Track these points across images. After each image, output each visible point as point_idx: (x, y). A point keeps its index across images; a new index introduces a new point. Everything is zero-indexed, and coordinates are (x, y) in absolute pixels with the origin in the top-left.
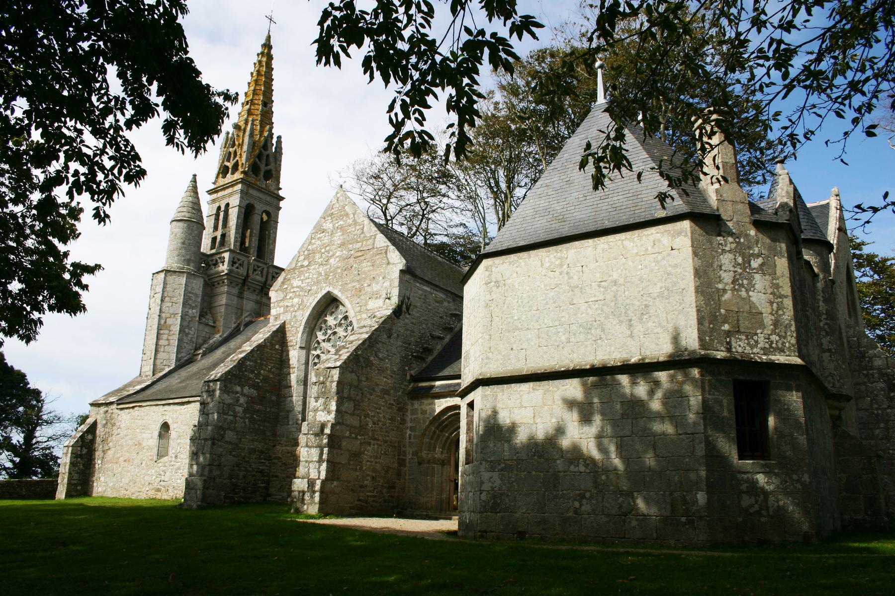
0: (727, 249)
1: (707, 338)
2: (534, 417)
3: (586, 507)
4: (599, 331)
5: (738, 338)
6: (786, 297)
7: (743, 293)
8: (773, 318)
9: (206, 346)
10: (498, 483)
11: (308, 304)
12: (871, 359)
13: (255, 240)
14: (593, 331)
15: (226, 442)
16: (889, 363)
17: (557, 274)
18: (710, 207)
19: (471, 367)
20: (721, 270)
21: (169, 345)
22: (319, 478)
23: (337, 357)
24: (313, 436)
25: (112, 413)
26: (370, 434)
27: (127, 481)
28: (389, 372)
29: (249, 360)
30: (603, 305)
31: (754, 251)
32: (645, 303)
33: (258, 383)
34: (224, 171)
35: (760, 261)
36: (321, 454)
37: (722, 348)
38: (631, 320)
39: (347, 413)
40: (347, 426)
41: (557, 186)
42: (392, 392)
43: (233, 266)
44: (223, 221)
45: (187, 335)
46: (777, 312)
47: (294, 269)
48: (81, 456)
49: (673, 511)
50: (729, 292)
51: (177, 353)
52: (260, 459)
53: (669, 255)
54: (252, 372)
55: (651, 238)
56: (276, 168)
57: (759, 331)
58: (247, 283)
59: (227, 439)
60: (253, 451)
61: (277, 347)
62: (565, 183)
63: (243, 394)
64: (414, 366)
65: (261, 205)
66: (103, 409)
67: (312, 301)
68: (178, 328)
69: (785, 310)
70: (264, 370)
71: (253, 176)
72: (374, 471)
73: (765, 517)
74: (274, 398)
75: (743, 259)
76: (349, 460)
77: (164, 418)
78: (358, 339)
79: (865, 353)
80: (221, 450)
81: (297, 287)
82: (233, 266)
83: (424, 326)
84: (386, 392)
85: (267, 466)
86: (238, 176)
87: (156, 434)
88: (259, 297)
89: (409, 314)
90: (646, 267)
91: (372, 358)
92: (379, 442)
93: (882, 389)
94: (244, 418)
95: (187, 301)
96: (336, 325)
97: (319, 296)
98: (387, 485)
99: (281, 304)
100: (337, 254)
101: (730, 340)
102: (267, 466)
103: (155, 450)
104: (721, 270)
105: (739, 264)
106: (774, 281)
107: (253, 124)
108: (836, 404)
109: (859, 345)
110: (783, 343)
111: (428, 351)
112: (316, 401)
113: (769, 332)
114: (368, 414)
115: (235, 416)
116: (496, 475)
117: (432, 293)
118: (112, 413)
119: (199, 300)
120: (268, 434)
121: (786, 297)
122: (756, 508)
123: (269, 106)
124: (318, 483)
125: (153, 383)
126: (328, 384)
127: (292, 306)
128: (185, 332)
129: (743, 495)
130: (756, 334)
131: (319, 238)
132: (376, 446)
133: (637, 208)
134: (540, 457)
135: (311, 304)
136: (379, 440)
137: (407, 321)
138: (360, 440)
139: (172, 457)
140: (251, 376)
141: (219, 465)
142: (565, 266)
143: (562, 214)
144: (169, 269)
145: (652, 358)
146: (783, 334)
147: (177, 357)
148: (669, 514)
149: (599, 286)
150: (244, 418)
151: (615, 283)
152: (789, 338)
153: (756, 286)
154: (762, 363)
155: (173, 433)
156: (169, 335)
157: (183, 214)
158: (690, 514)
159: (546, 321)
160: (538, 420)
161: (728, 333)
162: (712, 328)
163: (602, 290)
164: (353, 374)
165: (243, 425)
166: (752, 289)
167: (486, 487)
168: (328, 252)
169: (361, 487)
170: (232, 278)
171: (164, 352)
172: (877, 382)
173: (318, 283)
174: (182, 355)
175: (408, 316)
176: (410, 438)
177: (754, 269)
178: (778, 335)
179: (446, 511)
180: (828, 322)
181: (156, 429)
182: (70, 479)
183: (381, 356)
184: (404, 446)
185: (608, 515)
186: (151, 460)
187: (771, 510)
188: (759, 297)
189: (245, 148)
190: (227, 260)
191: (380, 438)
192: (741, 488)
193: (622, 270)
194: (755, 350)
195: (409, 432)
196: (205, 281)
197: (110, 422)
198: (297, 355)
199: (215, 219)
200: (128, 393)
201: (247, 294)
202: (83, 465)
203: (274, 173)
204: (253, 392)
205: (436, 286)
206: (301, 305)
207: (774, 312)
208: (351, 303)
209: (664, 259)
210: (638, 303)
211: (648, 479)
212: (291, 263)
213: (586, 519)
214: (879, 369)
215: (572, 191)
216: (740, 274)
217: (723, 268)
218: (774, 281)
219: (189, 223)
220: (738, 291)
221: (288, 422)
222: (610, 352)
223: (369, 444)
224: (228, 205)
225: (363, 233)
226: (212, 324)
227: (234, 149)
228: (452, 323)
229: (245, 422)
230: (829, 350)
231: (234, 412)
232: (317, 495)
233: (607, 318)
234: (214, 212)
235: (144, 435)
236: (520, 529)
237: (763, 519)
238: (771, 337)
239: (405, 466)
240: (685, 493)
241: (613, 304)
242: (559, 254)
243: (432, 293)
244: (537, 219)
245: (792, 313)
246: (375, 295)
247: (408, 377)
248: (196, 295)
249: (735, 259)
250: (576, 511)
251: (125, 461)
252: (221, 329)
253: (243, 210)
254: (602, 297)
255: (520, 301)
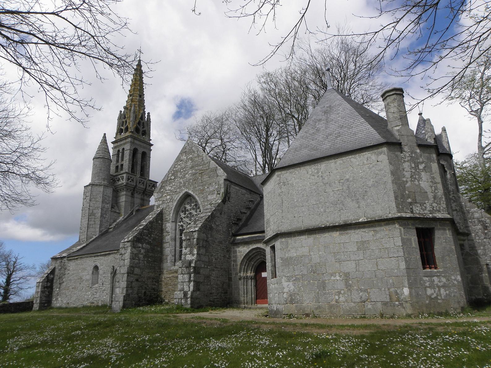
0: (406, 160)
1: (400, 206)
2: (310, 251)
3: (342, 299)
4: (341, 206)
5: (416, 206)
6: (439, 183)
7: (416, 182)
8: (433, 194)
9: (115, 223)
10: (292, 287)
11: (175, 199)
12: (473, 213)
13: (139, 167)
14: (338, 206)
15: (135, 274)
16: (483, 215)
17: (316, 177)
18: (396, 139)
19: (272, 227)
20: (404, 171)
21: (95, 224)
22: (189, 291)
23: (195, 225)
24: (185, 268)
25: (65, 263)
26: (214, 265)
27: (74, 299)
28: (221, 232)
29: (145, 229)
30: (342, 192)
31: (420, 160)
32: (365, 190)
33: (151, 241)
34: (120, 131)
35: (423, 165)
36: (190, 277)
37: (409, 211)
38: (358, 199)
39: (202, 254)
40: (203, 261)
41: (311, 132)
42: (223, 242)
43: (128, 181)
44: (121, 157)
45: (105, 218)
46: (434, 191)
47: (167, 181)
48: (47, 287)
49: (390, 299)
50: (409, 182)
51: (100, 228)
52: (153, 282)
53: (376, 165)
54: (147, 236)
55: (366, 156)
56: (148, 130)
57: (426, 202)
58: (136, 189)
59: (135, 272)
60: (149, 278)
61: (159, 222)
62: (315, 131)
63: (143, 248)
64: (233, 228)
65: (141, 149)
66: (58, 262)
67: (177, 197)
68: (100, 214)
69: (438, 190)
70: (153, 235)
71: (136, 133)
72: (217, 285)
73: (440, 300)
74: (159, 249)
75: (415, 165)
76: (204, 280)
77: (95, 263)
78: (205, 216)
79: (469, 211)
80: (133, 278)
81: (168, 190)
82: (128, 181)
83: (237, 207)
84: (220, 242)
85: (156, 286)
86: (128, 134)
87: (91, 272)
88: (142, 196)
89: (229, 202)
90: (364, 171)
91: (213, 225)
92: (219, 269)
93: (480, 229)
94: (143, 261)
95: (104, 200)
96: (190, 209)
97: (181, 194)
98: (223, 292)
99: (160, 199)
100: (190, 172)
101: (412, 207)
102: (156, 286)
103: (90, 281)
104: (404, 171)
105: (413, 168)
106: (432, 175)
107: (135, 107)
108: (462, 238)
109: (466, 207)
110: (439, 207)
111: (239, 220)
112: (186, 250)
113: (432, 202)
114: (213, 255)
115: (139, 260)
116: (291, 283)
117: (240, 190)
118: (65, 263)
119: (111, 199)
120: (157, 268)
121: (439, 183)
122: (435, 295)
123: (142, 97)
124: (189, 293)
125: (87, 245)
126: (192, 240)
127: (167, 200)
128: (103, 216)
129: (427, 288)
130: (425, 203)
131: (179, 165)
132: (217, 271)
133: (356, 141)
134: (314, 273)
135: (177, 198)
136: (218, 268)
137: (228, 205)
138: (210, 268)
139: (100, 284)
140: (147, 238)
141: (131, 287)
142: (320, 173)
143: (316, 146)
144: (93, 183)
145: (371, 218)
146: (439, 203)
147: (99, 230)
148: (389, 301)
149: (339, 182)
150: (143, 261)
151: (348, 180)
152: (442, 205)
153: (423, 178)
154: (430, 218)
155: (101, 272)
156: (95, 219)
157: (100, 154)
158: (401, 300)
159: (312, 201)
160: (312, 253)
161: (411, 204)
162: (402, 201)
163: (341, 184)
164: (204, 234)
165: (144, 264)
166: (421, 180)
167: (286, 290)
168: (185, 171)
169: (211, 294)
170: (127, 187)
171: (92, 228)
172: (477, 225)
173: (180, 187)
174: (103, 229)
175: (229, 203)
176: (233, 266)
177: (421, 170)
178: (436, 203)
179: (254, 304)
180: (454, 195)
181: (90, 269)
182: (41, 301)
183: (217, 224)
184: (231, 270)
185: (355, 302)
186: (88, 287)
187: (443, 296)
188: (425, 183)
189: (131, 119)
190: (125, 178)
191: (219, 267)
192: (426, 285)
193: (351, 174)
194: (425, 212)
195: (233, 263)
196: (113, 189)
197: (64, 268)
198: (170, 225)
199: (117, 157)
200: (73, 251)
201: (136, 195)
202: (48, 292)
203: (147, 132)
204: (148, 246)
205: (242, 186)
206: (172, 200)
207: (433, 192)
208: (199, 197)
209: (373, 166)
210: (361, 190)
211: (375, 282)
212: (164, 178)
213: (343, 305)
214: (478, 219)
215: (320, 135)
216: (414, 173)
217: (405, 170)
218: (432, 175)
219: (104, 159)
220: (414, 181)
221: (167, 261)
222: (348, 216)
223: (214, 270)
224: (123, 149)
225: (203, 161)
226: (118, 212)
227: (125, 120)
228: (250, 205)
229: (144, 263)
230: (456, 210)
231: (138, 257)
232: (189, 300)
233: (345, 198)
234: (116, 153)
235: (83, 273)
236: (306, 312)
237: (439, 301)
238: (433, 204)
239: (232, 281)
240: (396, 289)
241: (347, 191)
242: (316, 167)
243: (240, 190)
244: (302, 150)
245: (442, 192)
246: (212, 193)
247: (231, 234)
248: (109, 197)
249: (411, 165)
250: (337, 301)
251: (73, 288)
252: (123, 214)
253: (132, 152)
254: (341, 188)
255: (297, 192)
